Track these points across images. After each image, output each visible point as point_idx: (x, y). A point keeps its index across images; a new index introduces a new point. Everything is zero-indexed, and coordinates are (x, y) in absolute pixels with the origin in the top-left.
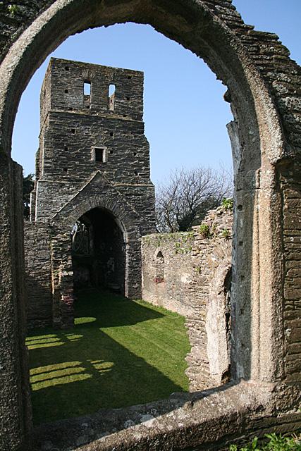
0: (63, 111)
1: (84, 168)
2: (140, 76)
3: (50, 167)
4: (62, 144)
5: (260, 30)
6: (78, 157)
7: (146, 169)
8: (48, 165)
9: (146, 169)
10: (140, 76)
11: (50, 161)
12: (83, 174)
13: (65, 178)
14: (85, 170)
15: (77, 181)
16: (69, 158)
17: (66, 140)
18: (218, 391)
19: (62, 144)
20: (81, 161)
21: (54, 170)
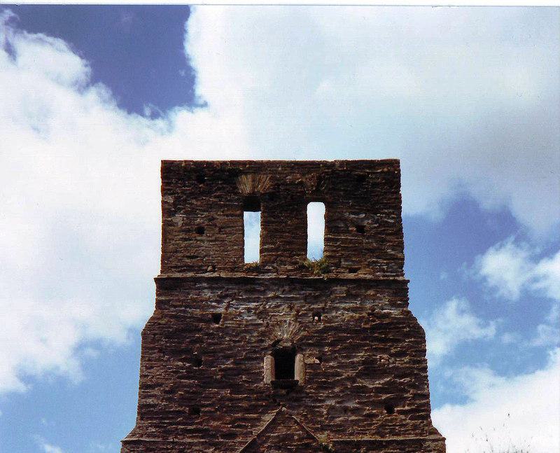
0: (190, 274)
1: (244, 404)
2: (164, 162)
3: (154, 406)
4: (188, 351)
5: (309, 160)
6: (228, 380)
7: (415, 396)
8: (150, 401)
9: (415, 396)
10: (164, 162)
11: (156, 391)
12: (244, 419)
13: (190, 432)
14: (247, 410)
15: (225, 436)
16: (207, 381)
17: (200, 340)
18: (236, 284)
19: (188, 351)
20: (236, 388)
21: (164, 414)
